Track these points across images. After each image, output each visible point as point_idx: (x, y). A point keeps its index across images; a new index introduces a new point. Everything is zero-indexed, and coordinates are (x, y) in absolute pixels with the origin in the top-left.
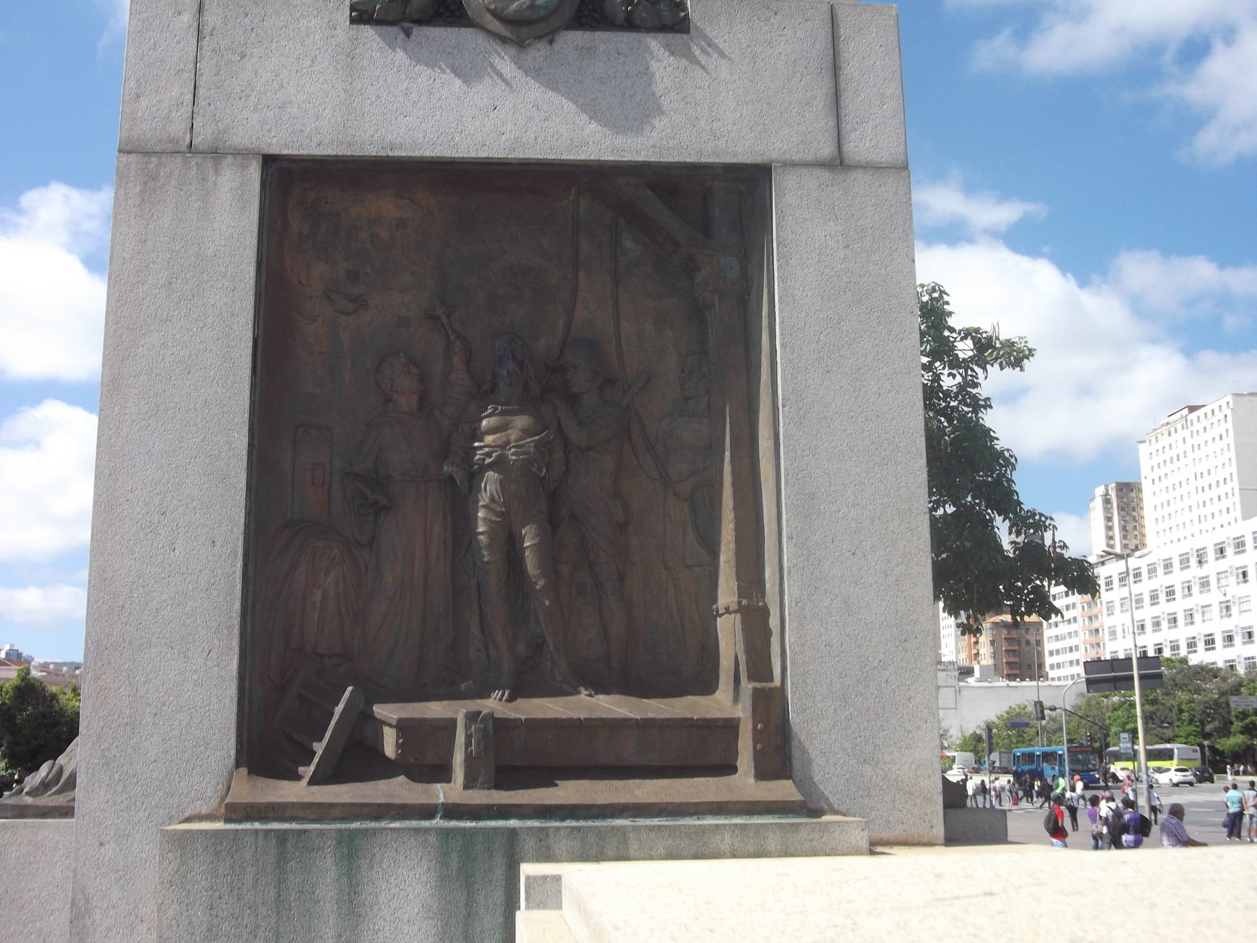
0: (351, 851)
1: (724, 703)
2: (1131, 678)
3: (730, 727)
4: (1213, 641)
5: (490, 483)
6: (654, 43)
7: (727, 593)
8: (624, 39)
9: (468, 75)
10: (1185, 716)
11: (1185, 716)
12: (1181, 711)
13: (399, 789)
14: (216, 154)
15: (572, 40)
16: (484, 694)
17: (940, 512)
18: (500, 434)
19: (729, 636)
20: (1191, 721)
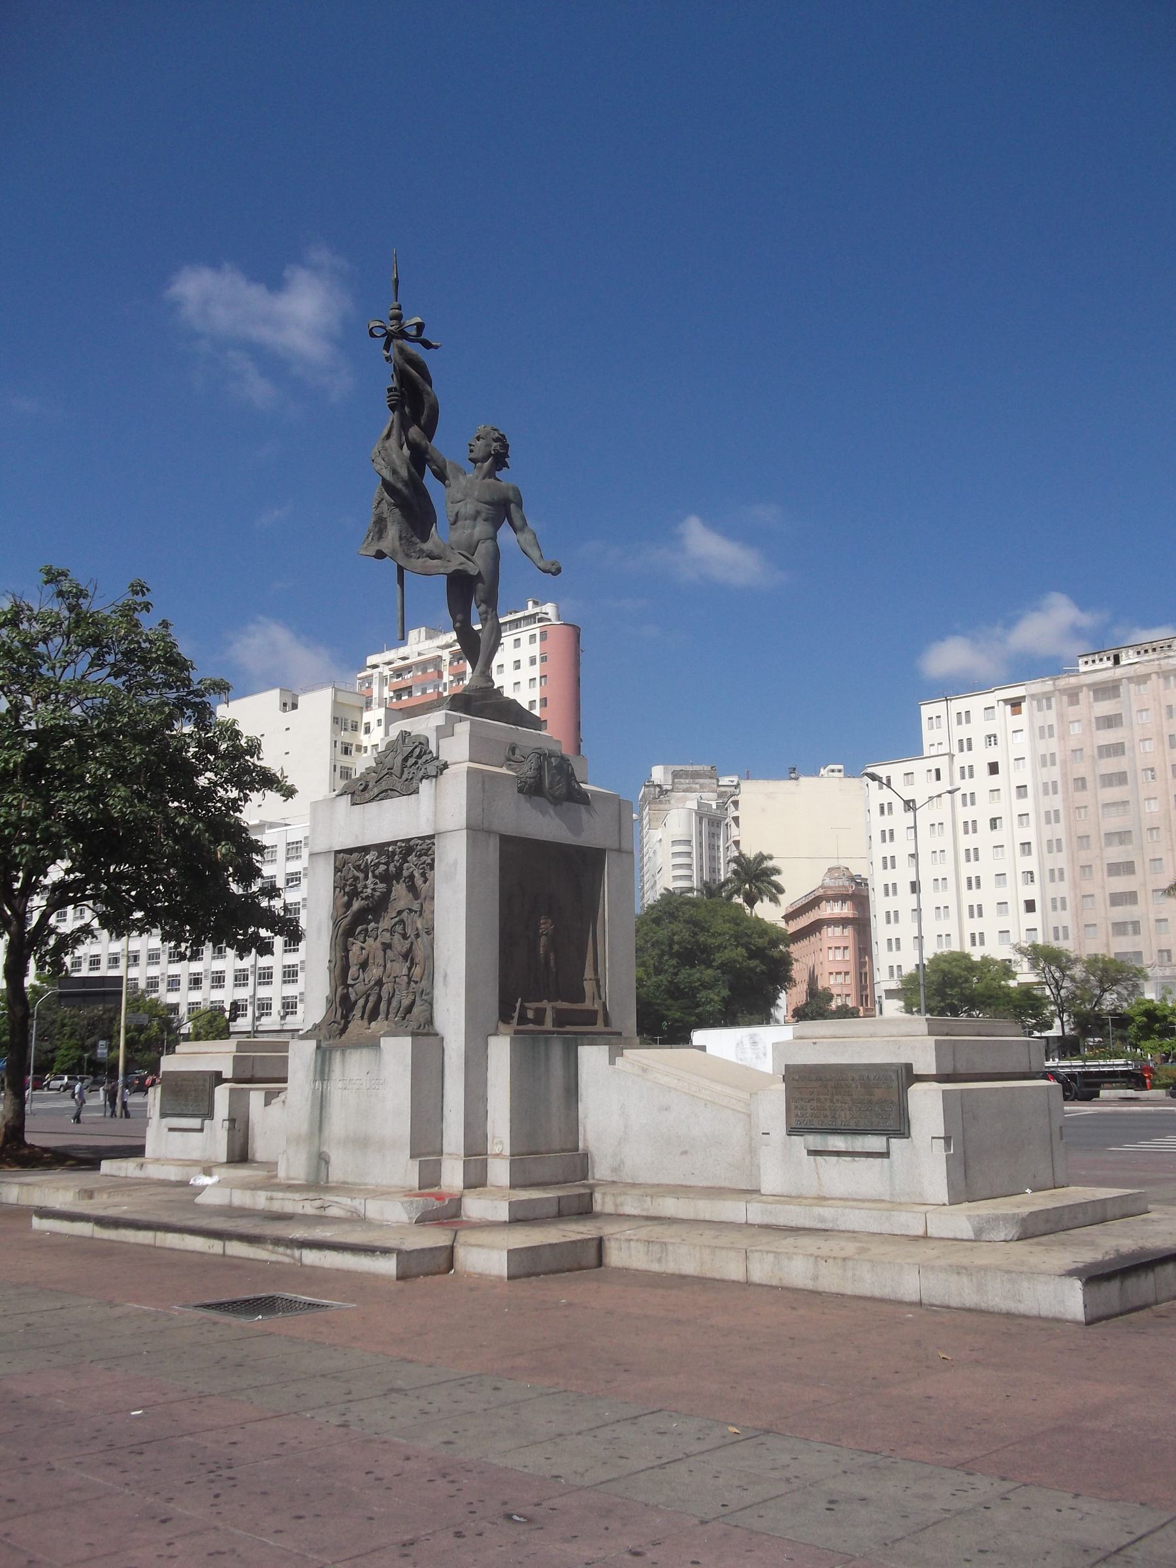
0: (547, 1041)
1: (588, 1005)
2: (120, 993)
3: (596, 1012)
4: (99, 962)
5: (543, 940)
6: (582, 807)
7: (588, 973)
8: (577, 805)
9: (544, 813)
10: (67, 1030)
11: (67, 1030)
12: (63, 1025)
13: (531, 1027)
14: (489, 832)
15: (566, 804)
16: (540, 1000)
17: (46, 853)
18: (545, 925)
19: (589, 987)
20: (72, 1035)
